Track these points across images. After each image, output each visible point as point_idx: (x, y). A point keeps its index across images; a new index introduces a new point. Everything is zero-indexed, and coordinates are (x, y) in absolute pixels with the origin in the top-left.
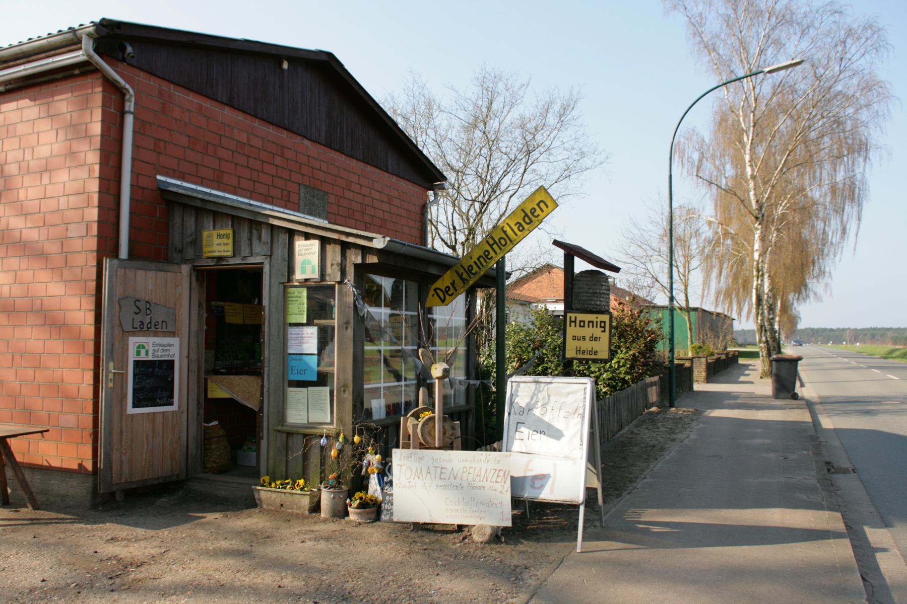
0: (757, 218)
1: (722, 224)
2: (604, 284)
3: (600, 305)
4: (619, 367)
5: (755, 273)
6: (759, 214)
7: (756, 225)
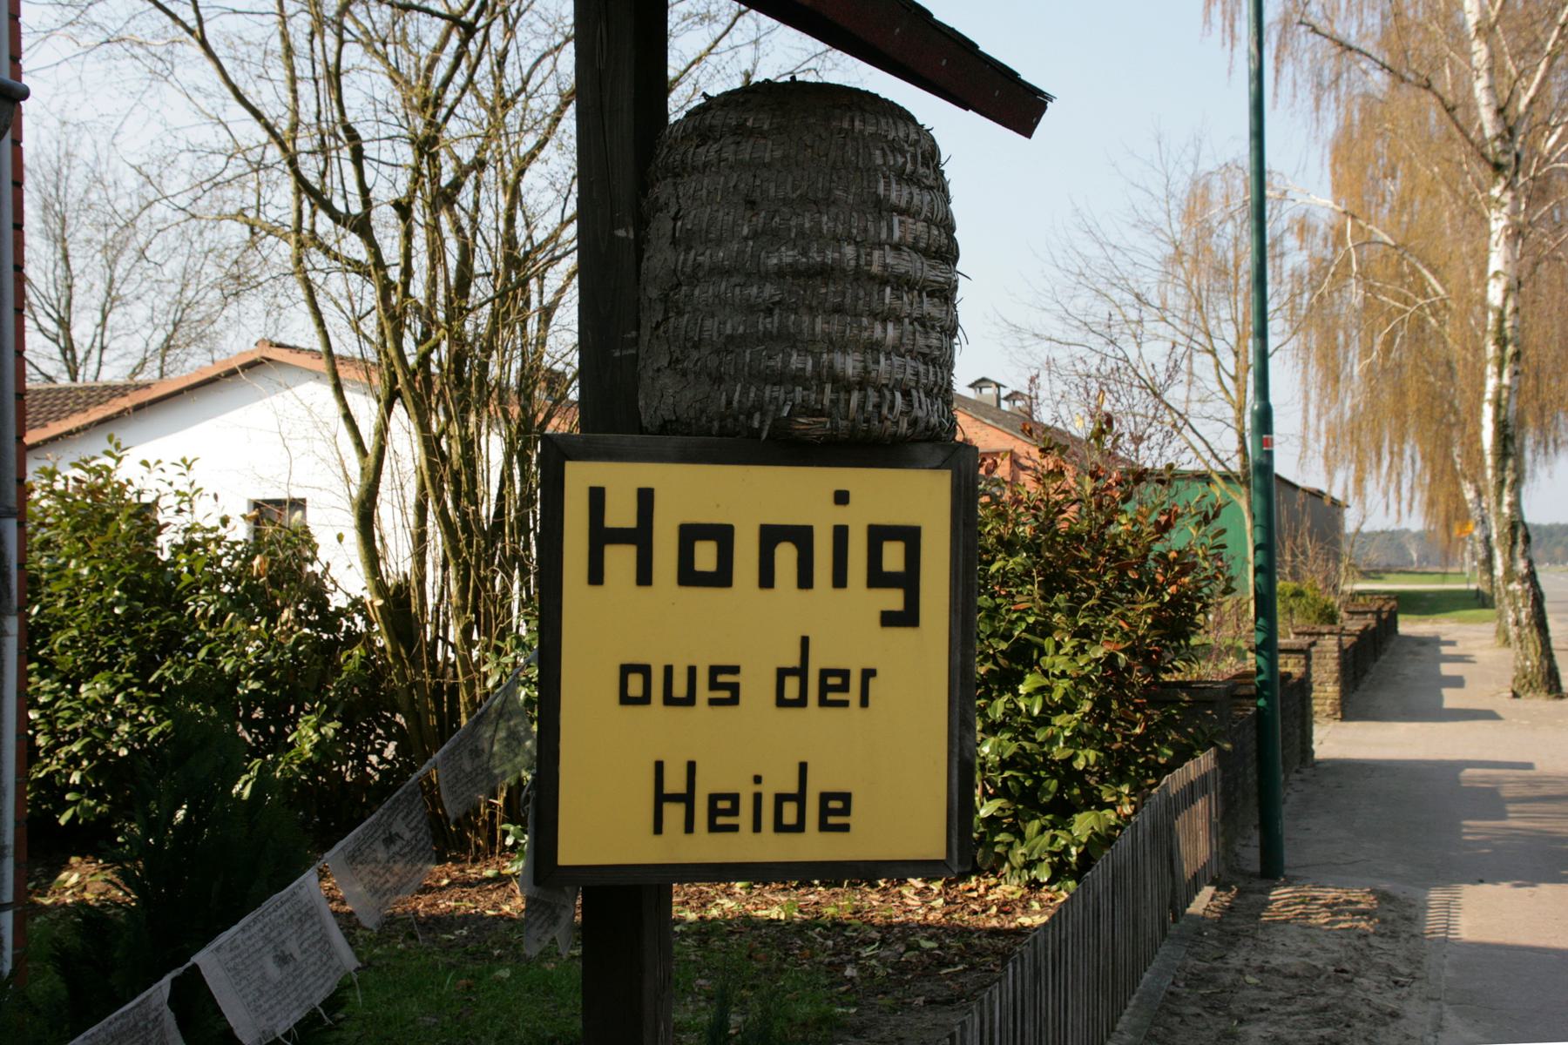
0: (1498, 168)
1: (1353, 217)
2: (898, 194)
3: (863, 384)
4: (1050, 710)
5: (1491, 349)
6: (1505, 152)
7: (1496, 192)
